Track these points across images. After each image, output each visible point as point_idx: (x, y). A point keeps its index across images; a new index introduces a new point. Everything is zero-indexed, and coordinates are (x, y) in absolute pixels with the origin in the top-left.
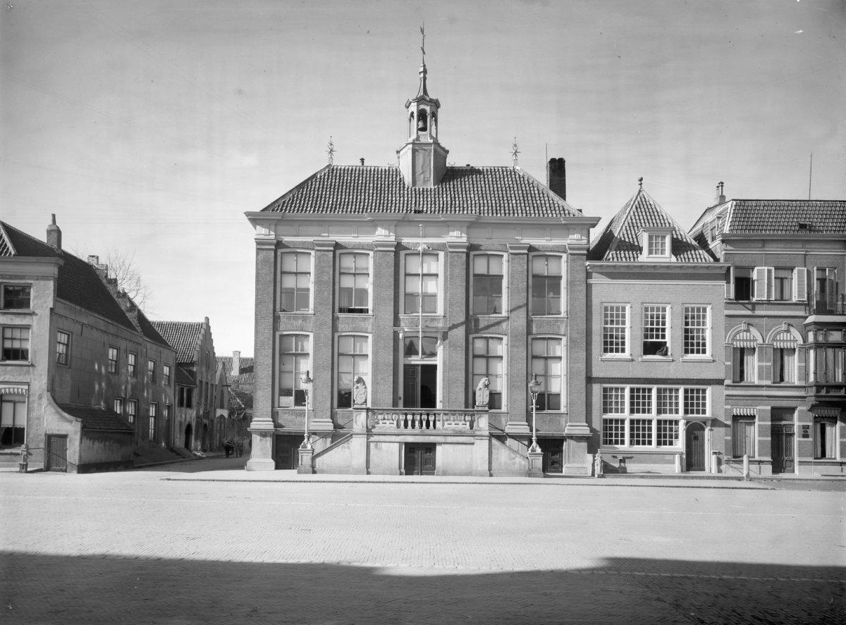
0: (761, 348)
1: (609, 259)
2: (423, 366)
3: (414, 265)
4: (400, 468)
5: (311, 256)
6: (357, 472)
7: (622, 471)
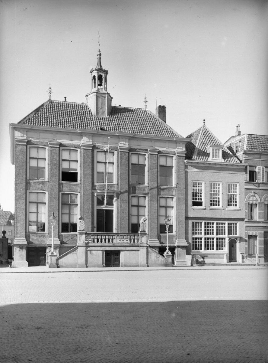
0: (260, 204)
1: (195, 160)
2: (106, 210)
3: (100, 157)
4: (103, 264)
5: (46, 150)
6: (81, 266)
7: (202, 264)
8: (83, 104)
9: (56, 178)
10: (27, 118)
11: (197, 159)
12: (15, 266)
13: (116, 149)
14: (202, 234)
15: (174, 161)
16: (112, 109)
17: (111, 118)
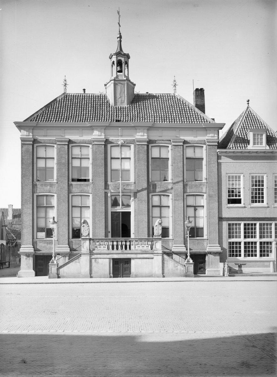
1: (231, 148)
2: (122, 212)
3: (116, 152)
6: (85, 277)
8: (101, 95)
9: (65, 178)
10: (35, 116)
11: (233, 147)
12: (20, 276)
13: (133, 142)
14: (272, 238)
15: (204, 152)
16: (135, 97)
17: (131, 107)
